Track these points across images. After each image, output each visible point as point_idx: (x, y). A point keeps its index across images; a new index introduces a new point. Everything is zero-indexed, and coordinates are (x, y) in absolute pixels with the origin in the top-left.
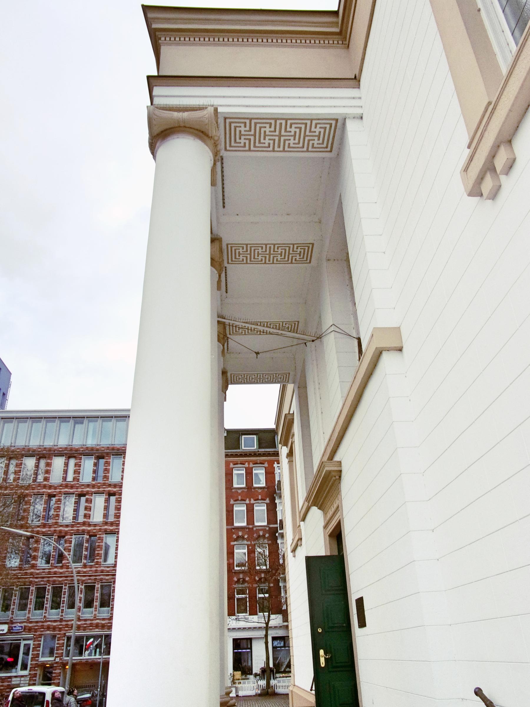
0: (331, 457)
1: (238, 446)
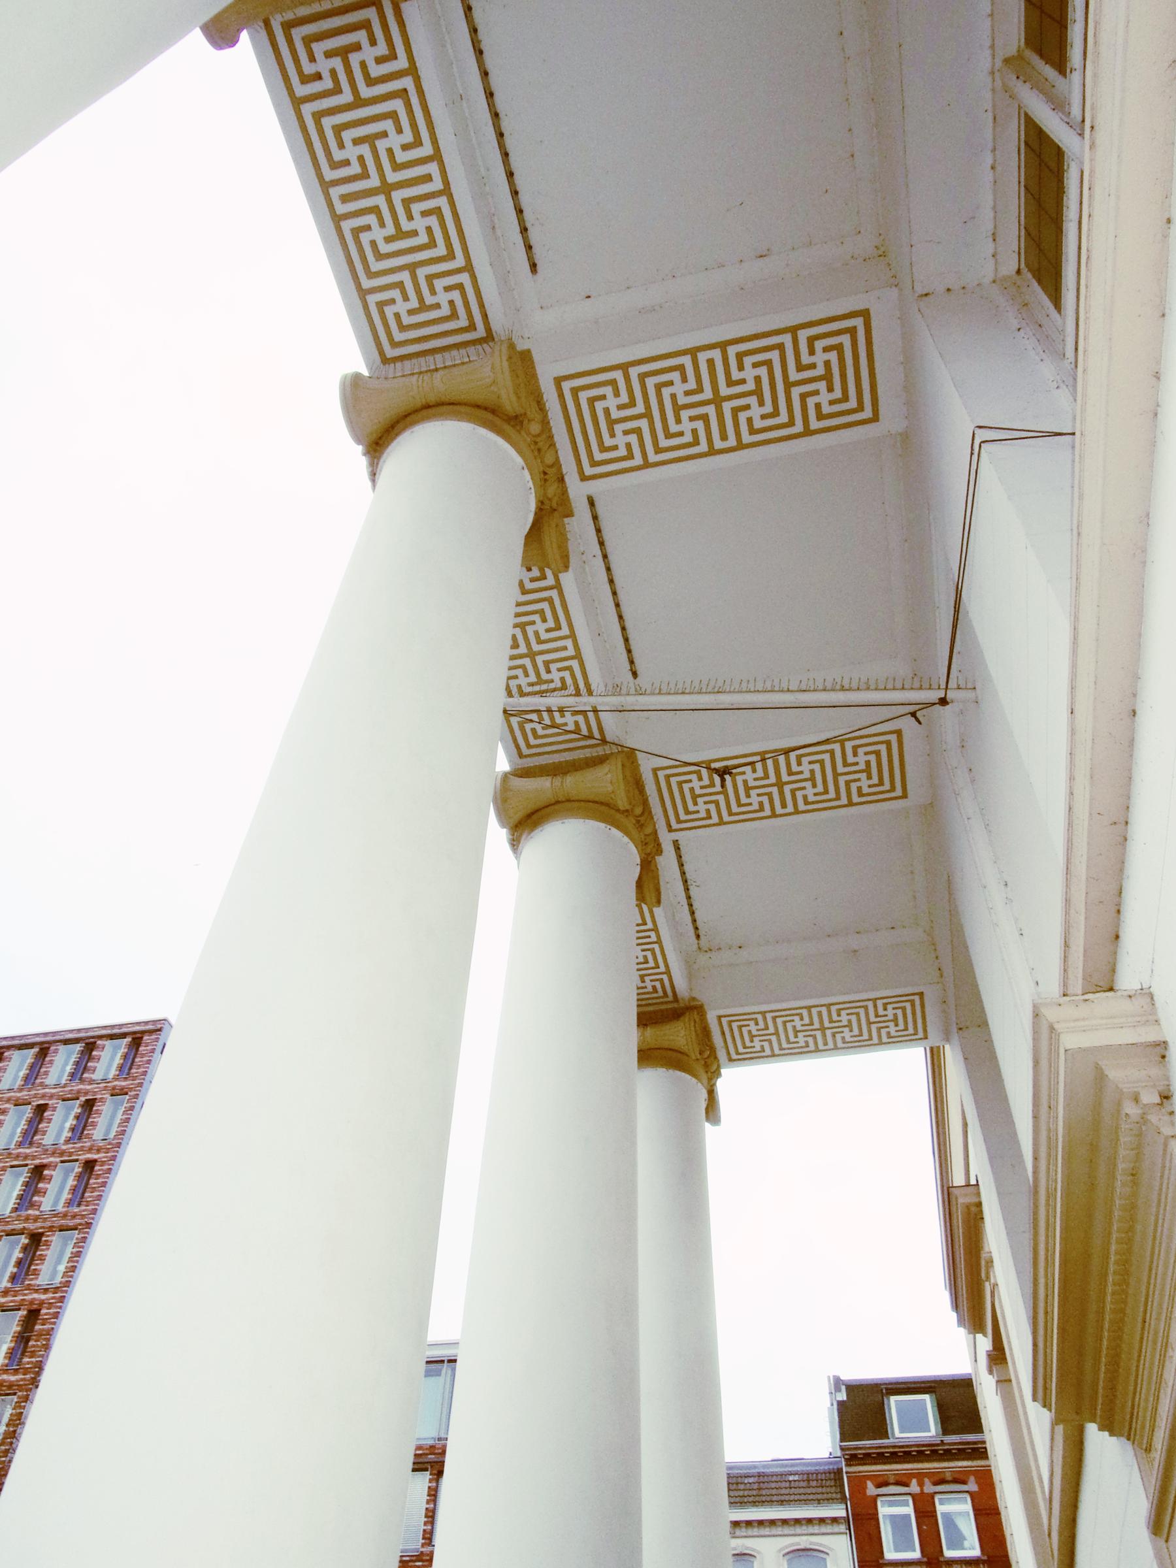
0: (1104, 981)
1: (880, 1427)
